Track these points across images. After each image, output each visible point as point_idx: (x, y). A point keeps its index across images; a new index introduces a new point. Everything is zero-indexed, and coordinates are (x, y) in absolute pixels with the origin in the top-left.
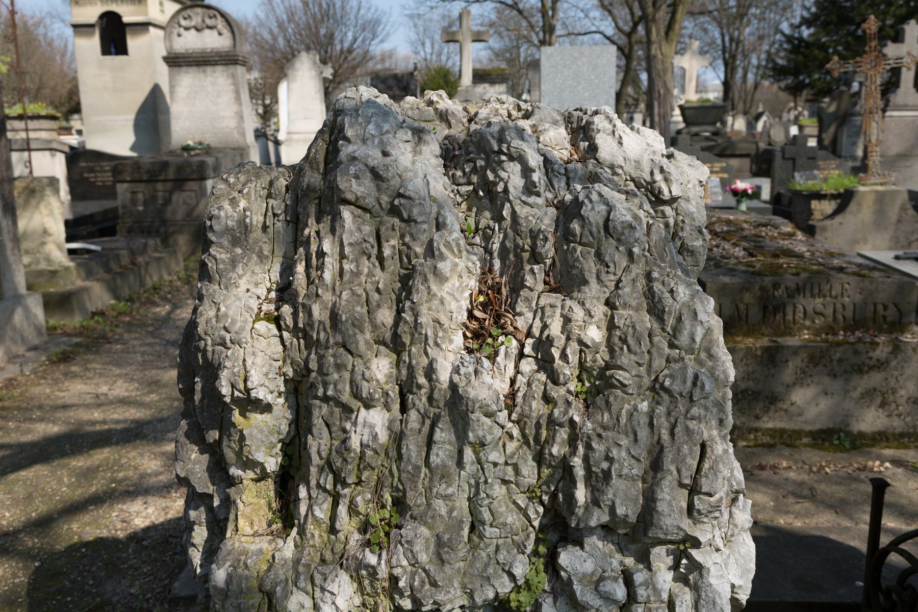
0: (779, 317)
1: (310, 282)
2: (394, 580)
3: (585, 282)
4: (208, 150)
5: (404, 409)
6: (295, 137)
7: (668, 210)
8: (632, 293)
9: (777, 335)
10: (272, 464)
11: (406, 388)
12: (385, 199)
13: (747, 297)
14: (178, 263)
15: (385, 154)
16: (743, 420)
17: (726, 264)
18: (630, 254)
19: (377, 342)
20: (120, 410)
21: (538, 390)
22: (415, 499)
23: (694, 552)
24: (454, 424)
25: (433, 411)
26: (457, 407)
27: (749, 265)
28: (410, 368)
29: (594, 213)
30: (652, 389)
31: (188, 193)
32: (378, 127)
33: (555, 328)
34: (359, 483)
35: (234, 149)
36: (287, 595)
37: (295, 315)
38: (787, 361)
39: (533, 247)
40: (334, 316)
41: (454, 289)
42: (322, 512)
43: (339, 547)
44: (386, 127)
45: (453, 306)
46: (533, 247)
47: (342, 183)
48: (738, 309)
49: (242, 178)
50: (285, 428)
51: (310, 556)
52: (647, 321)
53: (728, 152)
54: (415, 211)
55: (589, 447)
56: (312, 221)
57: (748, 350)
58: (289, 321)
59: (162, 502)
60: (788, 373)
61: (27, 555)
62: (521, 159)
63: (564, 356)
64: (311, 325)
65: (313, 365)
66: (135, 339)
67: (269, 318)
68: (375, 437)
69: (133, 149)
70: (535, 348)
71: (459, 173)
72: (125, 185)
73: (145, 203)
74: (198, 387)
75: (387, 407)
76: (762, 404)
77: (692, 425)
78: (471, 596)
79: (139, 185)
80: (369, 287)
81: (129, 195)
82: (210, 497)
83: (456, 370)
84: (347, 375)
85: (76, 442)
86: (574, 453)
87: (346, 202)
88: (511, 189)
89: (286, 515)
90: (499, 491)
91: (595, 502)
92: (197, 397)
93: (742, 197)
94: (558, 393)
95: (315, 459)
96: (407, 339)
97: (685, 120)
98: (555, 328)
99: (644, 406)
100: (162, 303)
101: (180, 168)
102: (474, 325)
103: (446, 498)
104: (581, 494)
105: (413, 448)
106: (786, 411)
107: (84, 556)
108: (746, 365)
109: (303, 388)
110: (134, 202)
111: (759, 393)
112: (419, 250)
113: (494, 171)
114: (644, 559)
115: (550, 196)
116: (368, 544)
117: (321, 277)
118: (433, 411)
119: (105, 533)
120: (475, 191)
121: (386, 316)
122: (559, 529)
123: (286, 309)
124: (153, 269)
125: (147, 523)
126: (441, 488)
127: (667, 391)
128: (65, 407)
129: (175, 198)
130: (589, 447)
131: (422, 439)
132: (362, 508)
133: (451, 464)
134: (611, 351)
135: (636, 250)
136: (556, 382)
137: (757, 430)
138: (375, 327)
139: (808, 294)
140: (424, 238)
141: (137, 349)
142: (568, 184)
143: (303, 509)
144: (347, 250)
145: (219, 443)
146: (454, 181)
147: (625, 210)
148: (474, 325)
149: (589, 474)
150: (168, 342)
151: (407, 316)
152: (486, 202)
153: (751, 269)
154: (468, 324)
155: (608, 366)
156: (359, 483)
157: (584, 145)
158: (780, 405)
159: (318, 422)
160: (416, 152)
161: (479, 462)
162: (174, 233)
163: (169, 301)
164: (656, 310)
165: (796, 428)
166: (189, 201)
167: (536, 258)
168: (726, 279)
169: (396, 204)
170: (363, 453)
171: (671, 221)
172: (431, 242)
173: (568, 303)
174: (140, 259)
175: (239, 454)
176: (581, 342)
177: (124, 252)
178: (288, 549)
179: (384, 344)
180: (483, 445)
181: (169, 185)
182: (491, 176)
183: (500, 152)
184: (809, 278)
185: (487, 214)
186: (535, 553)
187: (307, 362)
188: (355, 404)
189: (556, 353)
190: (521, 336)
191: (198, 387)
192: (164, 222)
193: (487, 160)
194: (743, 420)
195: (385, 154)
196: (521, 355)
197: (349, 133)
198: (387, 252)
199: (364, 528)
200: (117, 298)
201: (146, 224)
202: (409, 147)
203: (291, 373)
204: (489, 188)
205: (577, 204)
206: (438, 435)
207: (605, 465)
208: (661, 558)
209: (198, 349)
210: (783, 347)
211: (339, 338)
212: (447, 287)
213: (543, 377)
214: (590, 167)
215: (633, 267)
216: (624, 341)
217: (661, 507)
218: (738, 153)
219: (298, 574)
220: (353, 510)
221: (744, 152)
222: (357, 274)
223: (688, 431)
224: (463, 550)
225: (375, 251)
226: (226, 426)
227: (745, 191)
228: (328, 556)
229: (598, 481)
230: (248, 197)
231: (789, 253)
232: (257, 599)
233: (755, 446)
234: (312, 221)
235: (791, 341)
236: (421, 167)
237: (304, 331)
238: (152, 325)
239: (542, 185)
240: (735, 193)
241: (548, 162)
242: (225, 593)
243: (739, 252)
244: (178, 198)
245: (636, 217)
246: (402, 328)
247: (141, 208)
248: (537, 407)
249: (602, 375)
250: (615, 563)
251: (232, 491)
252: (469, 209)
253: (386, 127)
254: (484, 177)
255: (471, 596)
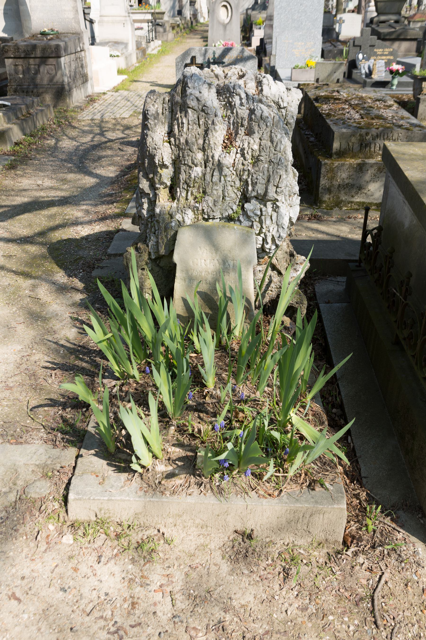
0: (368, 149)
1: (179, 131)
2: (203, 210)
3: (254, 133)
4: (58, 35)
5: (205, 167)
6: (105, 19)
7: (283, 110)
8: (266, 136)
9: (366, 158)
10: (169, 183)
11: (206, 162)
12: (200, 107)
13: (353, 139)
14: (51, 113)
15: (200, 92)
16: (346, 197)
17: (349, 122)
18: (267, 125)
19: (198, 149)
20: (53, 192)
21: (241, 162)
22: (208, 190)
23: (277, 203)
24: (219, 170)
25: (213, 167)
26: (220, 166)
27: (359, 123)
28: (208, 156)
29: (258, 113)
30: (269, 162)
31: (50, 66)
32: (198, 84)
33: (246, 146)
34: (194, 187)
35: (73, 34)
36: (176, 214)
37: (175, 141)
38: (368, 170)
39: (242, 122)
40: (187, 141)
41: (219, 134)
42: (184, 194)
43: (188, 204)
44: (200, 83)
45: (219, 139)
46: (242, 122)
47: (188, 102)
48: (349, 145)
49: (155, 97)
50: (172, 173)
51: (181, 206)
52: (269, 144)
53: (402, 37)
54: (209, 111)
55: (252, 176)
56: (178, 112)
57: (351, 164)
58: (174, 143)
59: (89, 227)
60: (368, 176)
61: (42, 244)
62: (239, 95)
63: (248, 153)
64: (180, 144)
65: (181, 155)
66: (44, 158)
67: (166, 141)
68: (198, 174)
69: (4, 31)
70: (241, 151)
71: (221, 98)
72: (10, 60)
73: (23, 73)
74: (147, 162)
75: (201, 166)
76: (355, 191)
77: (278, 170)
78: (222, 215)
79: (18, 60)
80: (196, 133)
81: (13, 67)
82: (149, 194)
83: (220, 156)
84: (190, 158)
85: (35, 206)
86: (249, 178)
87: (190, 108)
88: (236, 104)
89: (173, 196)
90: (230, 188)
91: (253, 190)
92: (146, 165)
93: (396, 75)
94: (246, 163)
95: (182, 181)
96: (206, 148)
97: (377, 10)
98: (246, 146)
99: (266, 166)
100: (49, 138)
101: (44, 49)
102: (225, 144)
103: (216, 190)
104: (250, 188)
105: (208, 177)
106: (366, 194)
107: (65, 244)
108: (349, 172)
109: (177, 162)
110: (17, 72)
111: (354, 185)
112: (210, 122)
113: (232, 98)
114: (265, 205)
115: (248, 106)
116: (196, 202)
117: (183, 130)
118: (213, 167)
119: (71, 237)
120: (226, 104)
121: (201, 142)
122: (245, 198)
123: (172, 139)
124: (39, 117)
125: (87, 234)
126: (215, 187)
127: (273, 162)
128: (25, 190)
129: (41, 69)
130: (252, 176)
131: (211, 175)
132: (194, 194)
133: (218, 181)
134: (260, 152)
135: (268, 124)
136: (245, 160)
137: (352, 202)
138: (198, 144)
139: (382, 138)
140: (211, 119)
141: (48, 163)
142: (253, 103)
143: (178, 194)
144: (190, 122)
145: (153, 178)
146: (220, 101)
147: (266, 112)
148: (225, 144)
149: (252, 183)
150: (62, 160)
151: (207, 141)
152: (229, 107)
153: (358, 125)
154: (124, 634)
155: (259, 156)
156: (194, 187)
157: (260, 88)
158: (363, 191)
159: (182, 171)
160: (209, 92)
161: (225, 180)
162: (42, 93)
163: (52, 137)
164: (272, 141)
165: (370, 202)
166: (50, 72)
167: (242, 126)
168: (344, 130)
169: (204, 110)
170: (195, 179)
171: (284, 114)
172: (213, 120)
173: (250, 138)
174: (32, 111)
175: (159, 181)
176: (252, 149)
177: (23, 106)
178: (175, 205)
179: (200, 149)
180: (226, 176)
181: (37, 60)
182: (231, 100)
183: (233, 92)
184: (383, 130)
185: (229, 111)
186: (239, 205)
187: (179, 154)
188: (193, 166)
189: (246, 152)
190: (237, 148)
191: (147, 162)
192: (36, 86)
193: (230, 94)
194: (346, 197)
195: (200, 92)
196: (237, 153)
197: (190, 85)
198: (201, 123)
199: (196, 198)
200: (25, 135)
201: (25, 87)
202: (207, 90)
203: (174, 158)
204: (230, 103)
205: (254, 110)
206: (215, 174)
207: (256, 180)
208: (269, 204)
209: (147, 150)
210: (366, 163)
211: (188, 147)
212: (218, 133)
213: (242, 158)
214: (260, 97)
215: (267, 129)
216: (263, 149)
217: (269, 191)
218: (409, 37)
219: (178, 210)
220: (192, 194)
221: (413, 37)
222: (193, 129)
223: (277, 172)
224: (220, 203)
225: (197, 123)
226: (155, 173)
227: (398, 70)
228: (186, 206)
229: (254, 184)
230: (158, 104)
231: (379, 117)
232: (168, 216)
233: (350, 210)
234: (178, 112)
235: (371, 161)
236: (210, 97)
237: (178, 145)
238: (49, 150)
239: (245, 104)
240: (391, 72)
241: (247, 95)
242: (160, 215)
243: (357, 116)
244: (44, 69)
245: (270, 114)
246: (205, 145)
247: (21, 76)
248: (241, 167)
249: (257, 158)
250: (258, 207)
251: (157, 191)
252: (224, 109)
253: (200, 83)
254: (229, 100)
255: (222, 215)
